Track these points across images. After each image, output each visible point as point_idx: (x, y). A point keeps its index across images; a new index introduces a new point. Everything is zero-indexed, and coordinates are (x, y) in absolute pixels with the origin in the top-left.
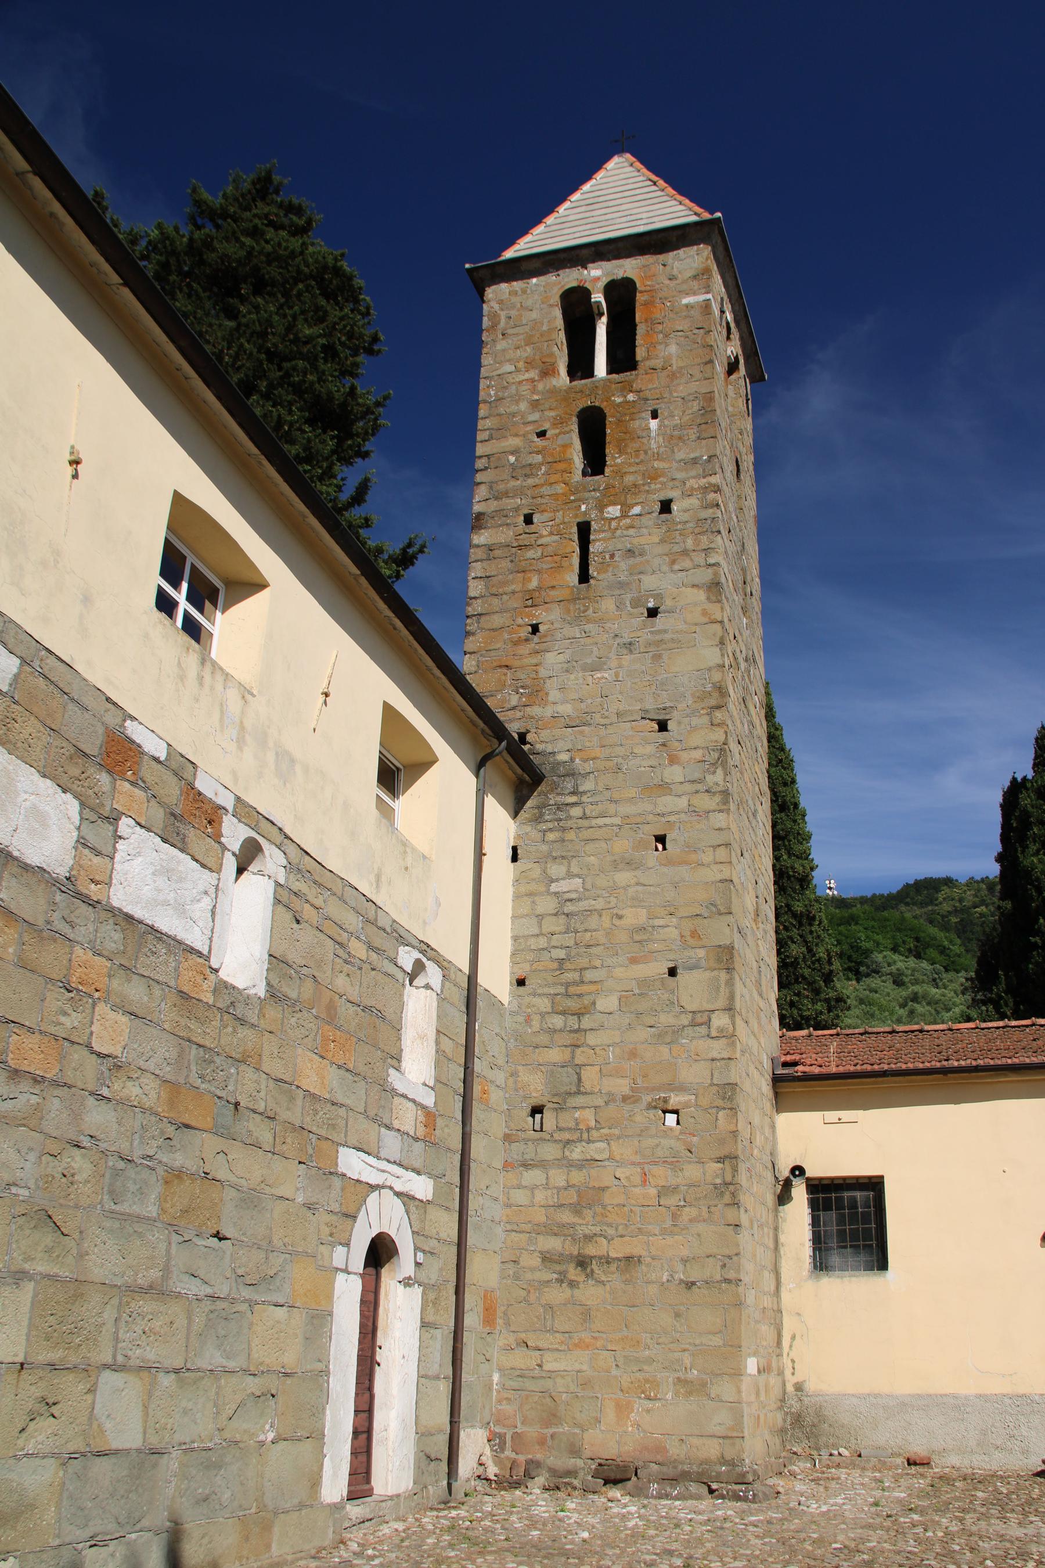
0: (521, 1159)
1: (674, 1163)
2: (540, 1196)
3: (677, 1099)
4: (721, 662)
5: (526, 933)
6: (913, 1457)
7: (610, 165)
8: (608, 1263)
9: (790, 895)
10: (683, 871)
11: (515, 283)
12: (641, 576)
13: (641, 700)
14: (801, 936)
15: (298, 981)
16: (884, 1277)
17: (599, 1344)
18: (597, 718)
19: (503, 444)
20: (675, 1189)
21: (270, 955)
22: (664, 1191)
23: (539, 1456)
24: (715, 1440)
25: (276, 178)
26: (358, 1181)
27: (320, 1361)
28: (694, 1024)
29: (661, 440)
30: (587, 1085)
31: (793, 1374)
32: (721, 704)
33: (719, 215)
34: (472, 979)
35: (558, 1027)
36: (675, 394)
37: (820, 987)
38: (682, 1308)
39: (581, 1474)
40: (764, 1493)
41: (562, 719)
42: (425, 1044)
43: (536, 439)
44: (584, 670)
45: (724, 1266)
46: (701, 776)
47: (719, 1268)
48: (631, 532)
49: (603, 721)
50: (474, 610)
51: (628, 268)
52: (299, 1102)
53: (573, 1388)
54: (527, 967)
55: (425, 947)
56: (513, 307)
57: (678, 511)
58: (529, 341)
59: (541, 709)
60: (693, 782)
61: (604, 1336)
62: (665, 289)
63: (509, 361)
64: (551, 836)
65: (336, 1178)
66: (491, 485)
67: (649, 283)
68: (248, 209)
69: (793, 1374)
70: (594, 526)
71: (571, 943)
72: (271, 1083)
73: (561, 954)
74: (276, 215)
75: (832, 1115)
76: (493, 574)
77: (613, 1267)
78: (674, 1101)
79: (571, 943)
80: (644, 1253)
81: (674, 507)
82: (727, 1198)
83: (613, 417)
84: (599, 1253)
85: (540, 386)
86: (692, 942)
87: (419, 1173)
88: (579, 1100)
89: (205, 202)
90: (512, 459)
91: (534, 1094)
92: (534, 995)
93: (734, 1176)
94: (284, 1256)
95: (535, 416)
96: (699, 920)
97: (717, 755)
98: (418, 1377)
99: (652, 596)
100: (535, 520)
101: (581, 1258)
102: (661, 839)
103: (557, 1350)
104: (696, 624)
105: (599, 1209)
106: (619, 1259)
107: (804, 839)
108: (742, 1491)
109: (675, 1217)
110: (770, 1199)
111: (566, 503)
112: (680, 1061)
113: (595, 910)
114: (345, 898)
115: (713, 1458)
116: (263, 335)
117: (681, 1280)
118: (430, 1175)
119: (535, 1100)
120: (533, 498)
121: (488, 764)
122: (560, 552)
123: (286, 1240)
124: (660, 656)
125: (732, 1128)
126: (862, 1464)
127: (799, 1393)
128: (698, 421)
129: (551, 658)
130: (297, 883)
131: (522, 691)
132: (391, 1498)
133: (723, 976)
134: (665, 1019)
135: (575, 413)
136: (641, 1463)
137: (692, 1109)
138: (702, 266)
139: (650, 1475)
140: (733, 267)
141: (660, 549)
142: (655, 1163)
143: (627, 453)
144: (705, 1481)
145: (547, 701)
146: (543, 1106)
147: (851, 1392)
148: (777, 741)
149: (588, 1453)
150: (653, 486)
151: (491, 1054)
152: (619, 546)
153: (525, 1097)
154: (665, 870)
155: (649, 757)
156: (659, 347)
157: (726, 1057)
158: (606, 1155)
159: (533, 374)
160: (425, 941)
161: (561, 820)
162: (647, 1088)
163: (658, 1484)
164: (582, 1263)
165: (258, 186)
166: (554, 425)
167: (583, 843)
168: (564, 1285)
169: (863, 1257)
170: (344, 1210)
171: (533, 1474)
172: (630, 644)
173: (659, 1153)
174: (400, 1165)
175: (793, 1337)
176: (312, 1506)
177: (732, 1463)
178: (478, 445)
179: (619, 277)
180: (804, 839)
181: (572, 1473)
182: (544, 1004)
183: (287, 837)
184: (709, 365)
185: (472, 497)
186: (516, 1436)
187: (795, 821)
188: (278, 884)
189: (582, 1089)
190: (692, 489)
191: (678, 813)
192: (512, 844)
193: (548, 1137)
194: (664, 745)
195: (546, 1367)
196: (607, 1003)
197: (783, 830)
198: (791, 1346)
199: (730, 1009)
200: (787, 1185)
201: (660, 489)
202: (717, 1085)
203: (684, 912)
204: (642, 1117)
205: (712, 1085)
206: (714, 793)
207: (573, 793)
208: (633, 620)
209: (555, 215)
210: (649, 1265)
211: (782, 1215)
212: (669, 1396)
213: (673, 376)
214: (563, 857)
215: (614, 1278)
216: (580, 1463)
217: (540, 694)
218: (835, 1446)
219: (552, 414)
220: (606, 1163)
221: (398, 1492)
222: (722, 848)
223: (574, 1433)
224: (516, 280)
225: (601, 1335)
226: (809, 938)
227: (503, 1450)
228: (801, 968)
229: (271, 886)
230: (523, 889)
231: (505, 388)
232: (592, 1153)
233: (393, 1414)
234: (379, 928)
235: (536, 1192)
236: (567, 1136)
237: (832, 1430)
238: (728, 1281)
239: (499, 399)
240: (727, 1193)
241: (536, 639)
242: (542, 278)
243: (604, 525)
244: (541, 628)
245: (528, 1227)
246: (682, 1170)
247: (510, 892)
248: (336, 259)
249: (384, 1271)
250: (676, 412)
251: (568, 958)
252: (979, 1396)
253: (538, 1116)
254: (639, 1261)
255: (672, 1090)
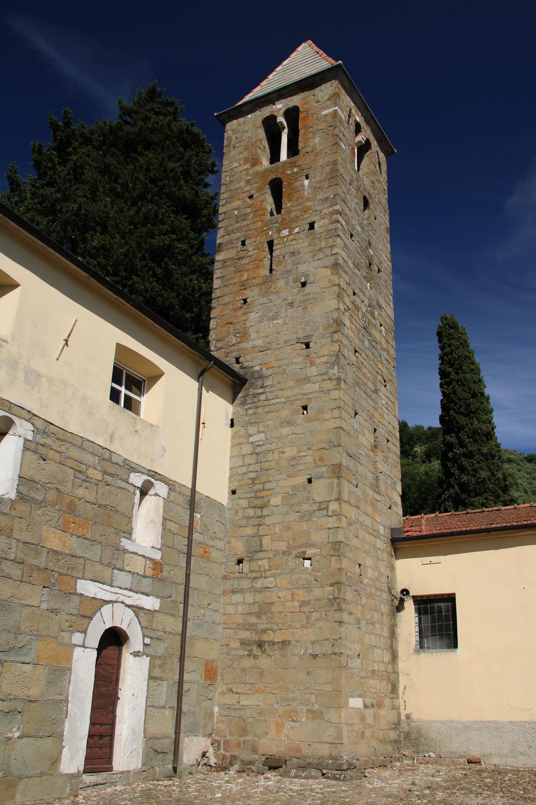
0: (231, 588)
1: (308, 588)
2: (240, 609)
3: (311, 551)
4: (338, 307)
5: (237, 465)
6: (471, 758)
7: (300, 48)
8: (273, 644)
9: (480, 444)
10: (316, 425)
11: (240, 119)
12: (298, 266)
13: (297, 333)
14: (488, 466)
15: (44, 491)
16: (456, 652)
17: (268, 690)
18: (274, 346)
19: (232, 205)
20: (308, 603)
21: (20, 477)
22: (303, 604)
23: (237, 753)
24: (327, 745)
25: (159, 89)
26: (94, 598)
27: (60, 694)
28: (320, 509)
29: (310, 190)
30: (265, 546)
31: (405, 709)
32: (337, 330)
33: (340, 62)
34: (193, 490)
35: (251, 515)
36: (317, 165)
37: (499, 494)
38: (311, 669)
39: (257, 764)
40: (351, 776)
41: (257, 348)
42: (154, 525)
43: (248, 200)
44: (269, 320)
45: (333, 645)
46: (326, 371)
47: (330, 646)
48: (294, 242)
49: (277, 347)
50: (216, 295)
51: (295, 100)
52: (44, 555)
53: (255, 715)
54: (236, 484)
55: (154, 474)
56: (239, 132)
57: (318, 227)
58: (246, 148)
59: (247, 344)
60: (322, 375)
61: (271, 685)
62: (314, 108)
63: (236, 161)
64: (250, 412)
65: (76, 597)
66: (226, 228)
67: (306, 107)
68: (142, 107)
69: (405, 709)
70: (275, 242)
71: (258, 469)
72: (21, 545)
73: (253, 475)
74: (159, 108)
75: (426, 560)
76: (225, 275)
77: (276, 647)
78: (309, 552)
79: (258, 469)
80: (292, 639)
81: (316, 226)
82: (335, 607)
83: (285, 182)
84: (269, 639)
85: (251, 172)
86: (319, 463)
87: (147, 595)
88: (261, 555)
89: (124, 108)
90: (236, 212)
91: (239, 553)
92: (240, 498)
93: (339, 594)
94: (30, 637)
95: (248, 188)
96: (324, 450)
97: (334, 359)
98: (146, 706)
99: (303, 276)
100: (247, 243)
101: (260, 643)
102: (305, 408)
103: (247, 694)
104: (325, 288)
105: (269, 615)
106: (278, 642)
107: (488, 412)
108: (338, 774)
109: (308, 618)
110: (385, 608)
111: (262, 231)
112: (312, 530)
113: (271, 450)
114: (84, 447)
115: (326, 755)
116: (148, 170)
117: (311, 654)
118: (157, 596)
119: (239, 556)
120: (246, 231)
121: (205, 374)
122: (258, 259)
123: (32, 628)
124: (306, 308)
125: (339, 566)
126: (441, 762)
127: (408, 720)
128: (329, 177)
129: (252, 316)
130: (43, 439)
131: (238, 335)
132: (122, 773)
133: (336, 481)
134: (305, 507)
135: (268, 183)
136: (288, 758)
137: (318, 557)
138: (333, 92)
139: (292, 765)
140: (357, 91)
141: (308, 250)
142: (299, 588)
143: (293, 200)
144: (320, 768)
145: (250, 339)
146: (243, 559)
147: (437, 720)
148: (470, 359)
149: (261, 752)
150: (305, 216)
151: (212, 531)
152: (288, 251)
153: (234, 555)
154: (306, 424)
155: (300, 363)
156: (310, 140)
157: (336, 526)
158: (273, 585)
159: (248, 166)
160: (153, 470)
161: (255, 402)
162: (295, 546)
163: (296, 769)
164: (260, 645)
165: (149, 95)
166: (257, 191)
167: (266, 414)
168: (251, 657)
169: (445, 641)
170: (82, 613)
171: (233, 763)
172: (292, 303)
173: (301, 582)
174: (131, 590)
175: (405, 688)
176: (52, 775)
177: (335, 758)
178: (220, 208)
179: (291, 106)
180: (488, 412)
181: (252, 763)
182: (244, 503)
183: (34, 415)
184: (335, 146)
185: (216, 236)
186: (226, 742)
187: (482, 403)
188: (26, 440)
189: (262, 548)
190: (325, 214)
191: (314, 392)
192: (231, 417)
193: (245, 576)
194: (307, 356)
195: (241, 704)
196: (276, 500)
197: (474, 408)
198: (404, 693)
199: (339, 500)
200: (402, 601)
201: (309, 217)
202: (331, 543)
203: (316, 447)
204: (292, 562)
205: (329, 543)
206: (333, 380)
207: (261, 387)
208: (293, 290)
209: (267, 80)
210: (294, 645)
211: (399, 617)
212: (304, 719)
213: (317, 155)
214: (256, 423)
215: (277, 653)
216: (257, 757)
217: (247, 336)
218: (428, 751)
219: (256, 185)
220: (274, 589)
221: (128, 770)
222: (336, 410)
223: (255, 740)
224: (240, 117)
225: (269, 685)
226: (492, 467)
227: (219, 749)
228: (487, 484)
229: (21, 442)
230: (235, 442)
231: (234, 175)
232: (266, 584)
233: (125, 726)
234: (114, 463)
235: (239, 606)
236: (254, 575)
237: (426, 741)
238: (335, 654)
239: (231, 182)
240: (336, 603)
241: (245, 306)
242: (253, 114)
243: (280, 241)
244: (248, 300)
245: (234, 626)
246: (312, 591)
247: (229, 444)
248: (188, 126)
249: (124, 648)
250: (318, 174)
251: (257, 478)
252: (510, 722)
253: (241, 565)
254: (289, 643)
255: (308, 547)
